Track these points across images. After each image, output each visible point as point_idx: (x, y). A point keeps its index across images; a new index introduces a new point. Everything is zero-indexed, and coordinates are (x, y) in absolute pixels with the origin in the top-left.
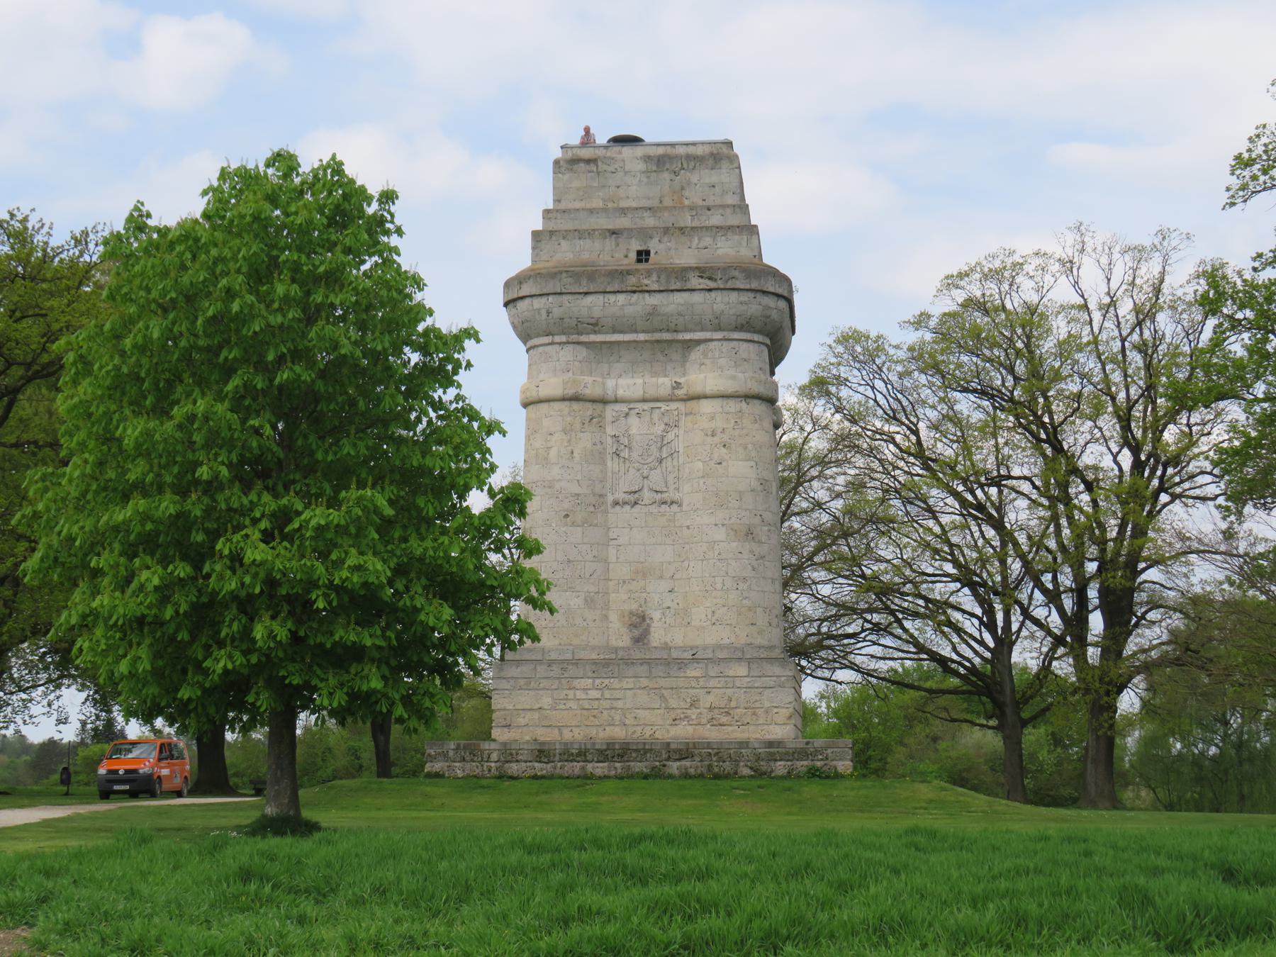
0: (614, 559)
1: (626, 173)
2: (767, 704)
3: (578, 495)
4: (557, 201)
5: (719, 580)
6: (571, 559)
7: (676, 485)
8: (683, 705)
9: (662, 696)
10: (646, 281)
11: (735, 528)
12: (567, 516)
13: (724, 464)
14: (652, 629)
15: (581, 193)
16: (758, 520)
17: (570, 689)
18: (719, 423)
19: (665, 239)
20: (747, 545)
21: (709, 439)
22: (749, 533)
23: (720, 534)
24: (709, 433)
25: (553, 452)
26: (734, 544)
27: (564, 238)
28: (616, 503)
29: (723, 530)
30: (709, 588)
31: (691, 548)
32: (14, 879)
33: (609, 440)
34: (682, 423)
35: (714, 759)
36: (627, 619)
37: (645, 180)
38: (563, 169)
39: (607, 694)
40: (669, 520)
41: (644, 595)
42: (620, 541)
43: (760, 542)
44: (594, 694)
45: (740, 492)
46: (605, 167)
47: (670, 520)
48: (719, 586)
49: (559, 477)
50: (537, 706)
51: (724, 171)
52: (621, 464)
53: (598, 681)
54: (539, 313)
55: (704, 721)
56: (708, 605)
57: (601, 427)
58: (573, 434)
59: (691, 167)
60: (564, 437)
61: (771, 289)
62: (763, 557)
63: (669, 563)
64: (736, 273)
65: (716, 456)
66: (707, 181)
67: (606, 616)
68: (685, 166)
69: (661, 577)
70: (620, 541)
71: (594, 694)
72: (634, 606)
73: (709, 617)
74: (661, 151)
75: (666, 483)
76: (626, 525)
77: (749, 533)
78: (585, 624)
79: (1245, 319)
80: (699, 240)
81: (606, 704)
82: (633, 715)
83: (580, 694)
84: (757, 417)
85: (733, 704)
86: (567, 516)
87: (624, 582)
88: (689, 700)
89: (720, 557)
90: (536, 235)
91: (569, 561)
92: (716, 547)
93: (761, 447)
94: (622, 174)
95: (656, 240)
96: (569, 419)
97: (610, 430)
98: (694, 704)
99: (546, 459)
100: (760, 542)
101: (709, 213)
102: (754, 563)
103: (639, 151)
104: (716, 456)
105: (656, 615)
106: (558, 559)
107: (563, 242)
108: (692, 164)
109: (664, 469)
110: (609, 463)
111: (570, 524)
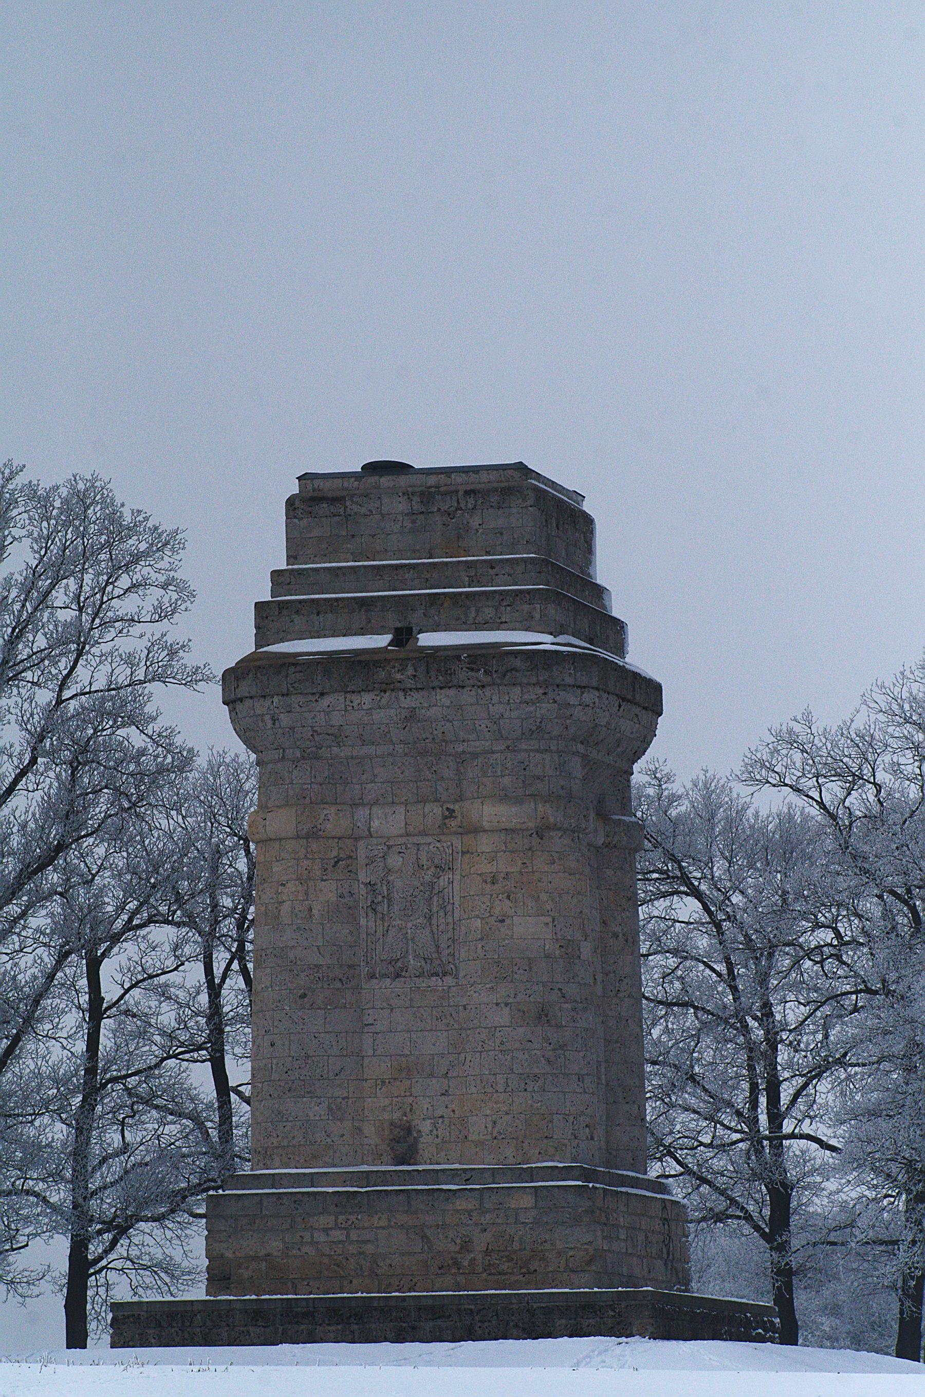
0: (370, 1053)
1: (383, 516)
2: (560, 1245)
3: (318, 966)
4: (292, 557)
5: (501, 1079)
6: (311, 1053)
7: (451, 950)
8: (453, 1248)
9: (424, 1237)
10: (399, 676)
11: (522, 1007)
12: (304, 996)
13: (508, 921)
14: (420, 1146)
15: (324, 546)
16: (555, 996)
17: (305, 1229)
18: (502, 865)
19: (433, 611)
20: (539, 1029)
21: (488, 887)
22: (542, 1015)
23: (503, 1017)
24: (489, 880)
25: (286, 908)
26: (521, 1030)
27: (297, 612)
28: (372, 976)
29: (507, 1010)
30: (489, 1090)
31: (468, 1036)
32: (838, 1306)
33: (363, 890)
34: (457, 865)
35: (477, 1318)
36: (387, 1132)
37: (408, 524)
38: (299, 512)
39: (354, 1236)
40: (442, 998)
41: (410, 1100)
42: (378, 1027)
43: (559, 1026)
44: (338, 1235)
45: (529, 959)
46: (356, 508)
47: (442, 998)
48: (501, 1088)
49: (293, 943)
50: (263, 1252)
51: (514, 510)
52: (379, 922)
53: (341, 1218)
54: (263, 721)
55: (479, 1269)
56: (488, 1112)
57: (352, 872)
58: (311, 883)
59: (470, 506)
60: (300, 888)
61: (569, 680)
62: (563, 1047)
63: (442, 1055)
64: (518, 663)
65: (497, 911)
66: (493, 524)
67: (360, 1130)
68: (462, 505)
69: (431, 1075)
70: (378, 1027)
71: (338, 1235)
72: (396, 1116)
73: (490, 1129)
74: (432, 480)
75: (437, 947)
76: (385, 1005)
77: (542, 1015)
78: (329, 1140)
79: (32, 1122)
80: (477, 611)
81: (352, 1249)
82: (388, 1262)
83: (321, 1237)
84: (556, 856)
85: (516, 1245)
86: (304, 996)
87: (383, 1082)
88: (458, 1241)
89: (503, 1048)
90: (260, 607)
91: (307, 1057)
92: (497, 1034)
93: (560, 895)
94: (378, 517)
95: (420, 612)
96: (306, 863)
97: (362, 876)
98: (466, 1246)
99: (276, 918)
100: (559, 1026)
101: (492, 572)
102: (549, 1054)
103: (403, 481)
104: (497, 911)
105: (426, 1127)
106: (293, 1054)
107: (297, 619)
108: (471, 501)
109: (434, 928)
110: (363, 922)
111: (307, 1006)
